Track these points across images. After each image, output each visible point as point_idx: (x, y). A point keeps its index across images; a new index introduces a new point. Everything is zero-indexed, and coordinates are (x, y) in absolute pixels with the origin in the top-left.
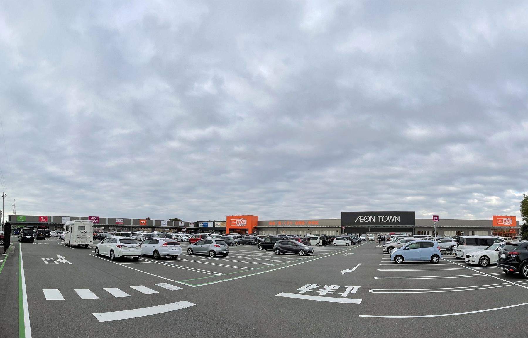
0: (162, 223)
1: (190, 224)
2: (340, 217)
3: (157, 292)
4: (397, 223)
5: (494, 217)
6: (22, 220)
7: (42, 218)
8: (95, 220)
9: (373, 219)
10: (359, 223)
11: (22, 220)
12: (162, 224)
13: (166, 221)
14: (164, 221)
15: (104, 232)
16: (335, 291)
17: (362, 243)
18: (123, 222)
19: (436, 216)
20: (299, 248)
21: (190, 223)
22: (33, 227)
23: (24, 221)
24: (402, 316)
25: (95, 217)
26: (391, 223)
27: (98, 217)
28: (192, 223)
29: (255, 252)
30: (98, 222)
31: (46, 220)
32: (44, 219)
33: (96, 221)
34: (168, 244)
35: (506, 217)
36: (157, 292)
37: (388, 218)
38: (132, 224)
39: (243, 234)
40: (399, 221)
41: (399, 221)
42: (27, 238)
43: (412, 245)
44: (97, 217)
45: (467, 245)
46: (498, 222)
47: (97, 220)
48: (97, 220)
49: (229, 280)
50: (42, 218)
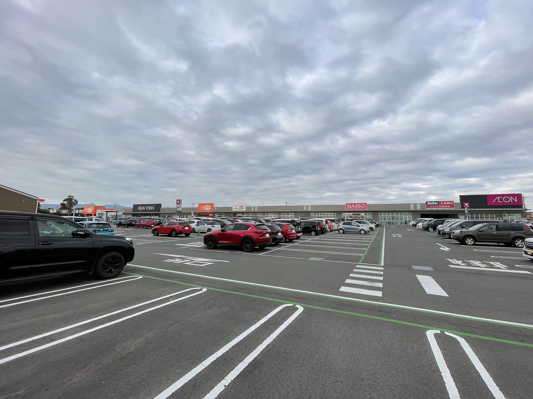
2: (132, 207)
3: (9, 269)
4: (153, 211)
5: (200, 205)
9: (514, 200)
10: (139, 211)
15: (350, 216)
17: (54, 223)
20: (264, 232)
24: (48, 331)
26: (150, 211)
27: (366, 204)
29: (327, 241)
34: (267, 230)
35: (206, 204)
36: (9, 269)
40: (516, 201)
41: (516, 201)
43: (94, 225)
46: (202, 209)
49: (226, 280)
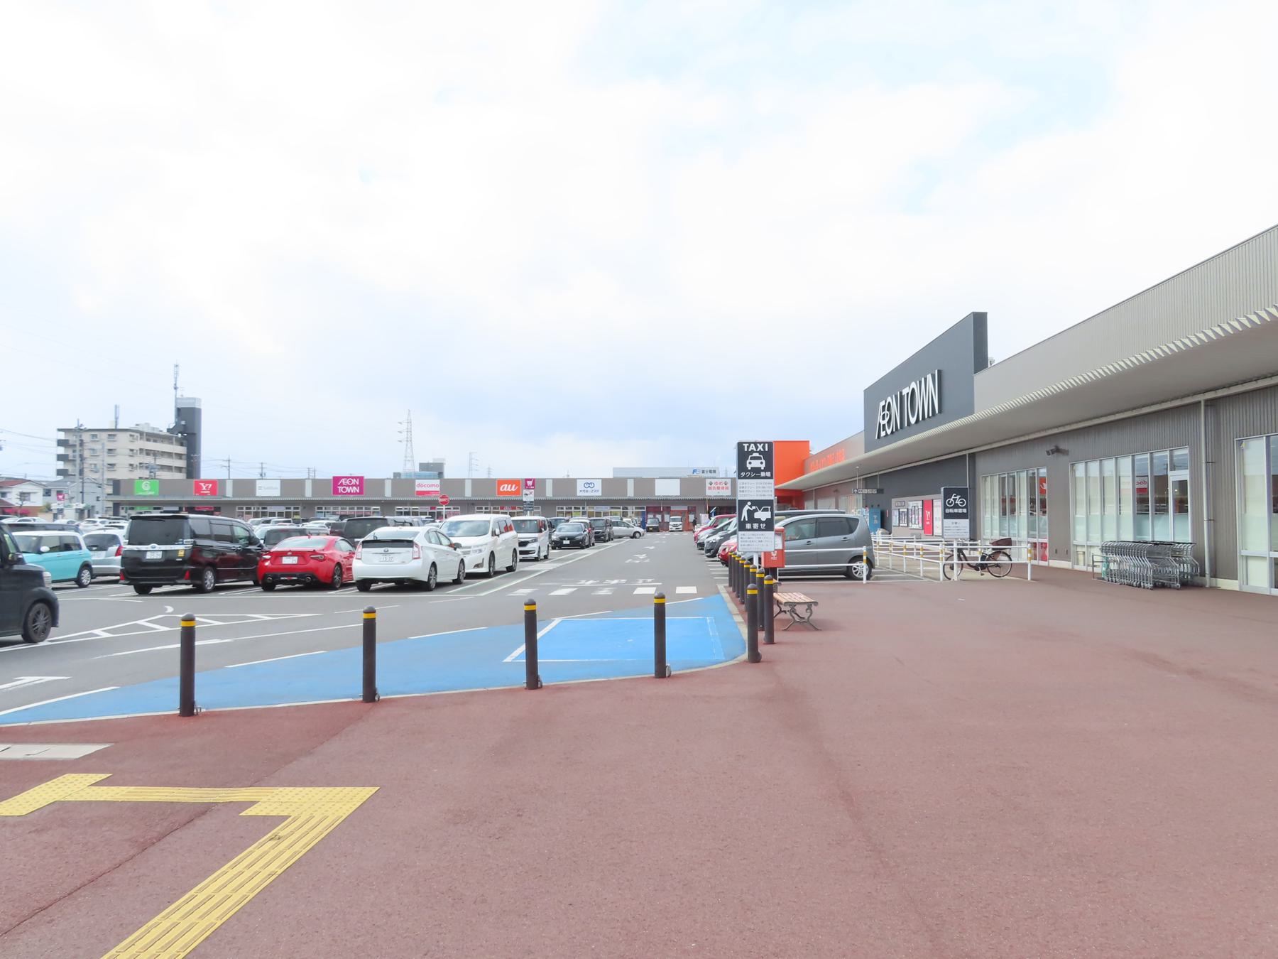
0: (580, 485)
1: (708, 485)
6: (150, 491)
7: (202, 484)
8: (352, 486)
11: (150, 491)
12: (581, 492)
13: (730, 480)
14: (589, 481)
16: (372, 588)
18: (438, 489)
19: (530, 480)
21: (708, 481)
22: (685, 508)
23: (153, 493)
25: (353, 478)
27: (361, 479)
28: (720, 480)
30: (361, 493)
31: (213, 492)
32: (207, 487)
33: (354, 488)
37: (347, 488)
38: (311, 496)
39: (1147, 496)
42: (149, 556)
44: (356, 478)
45: (1046, 508)
47: (356, 485)
48: (356, 485)
50: (202, 484)
